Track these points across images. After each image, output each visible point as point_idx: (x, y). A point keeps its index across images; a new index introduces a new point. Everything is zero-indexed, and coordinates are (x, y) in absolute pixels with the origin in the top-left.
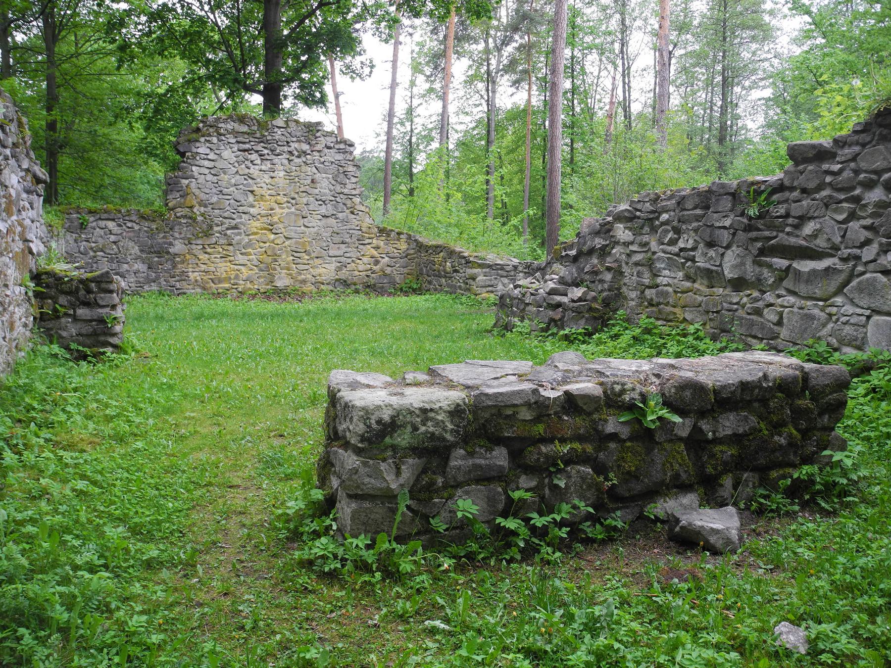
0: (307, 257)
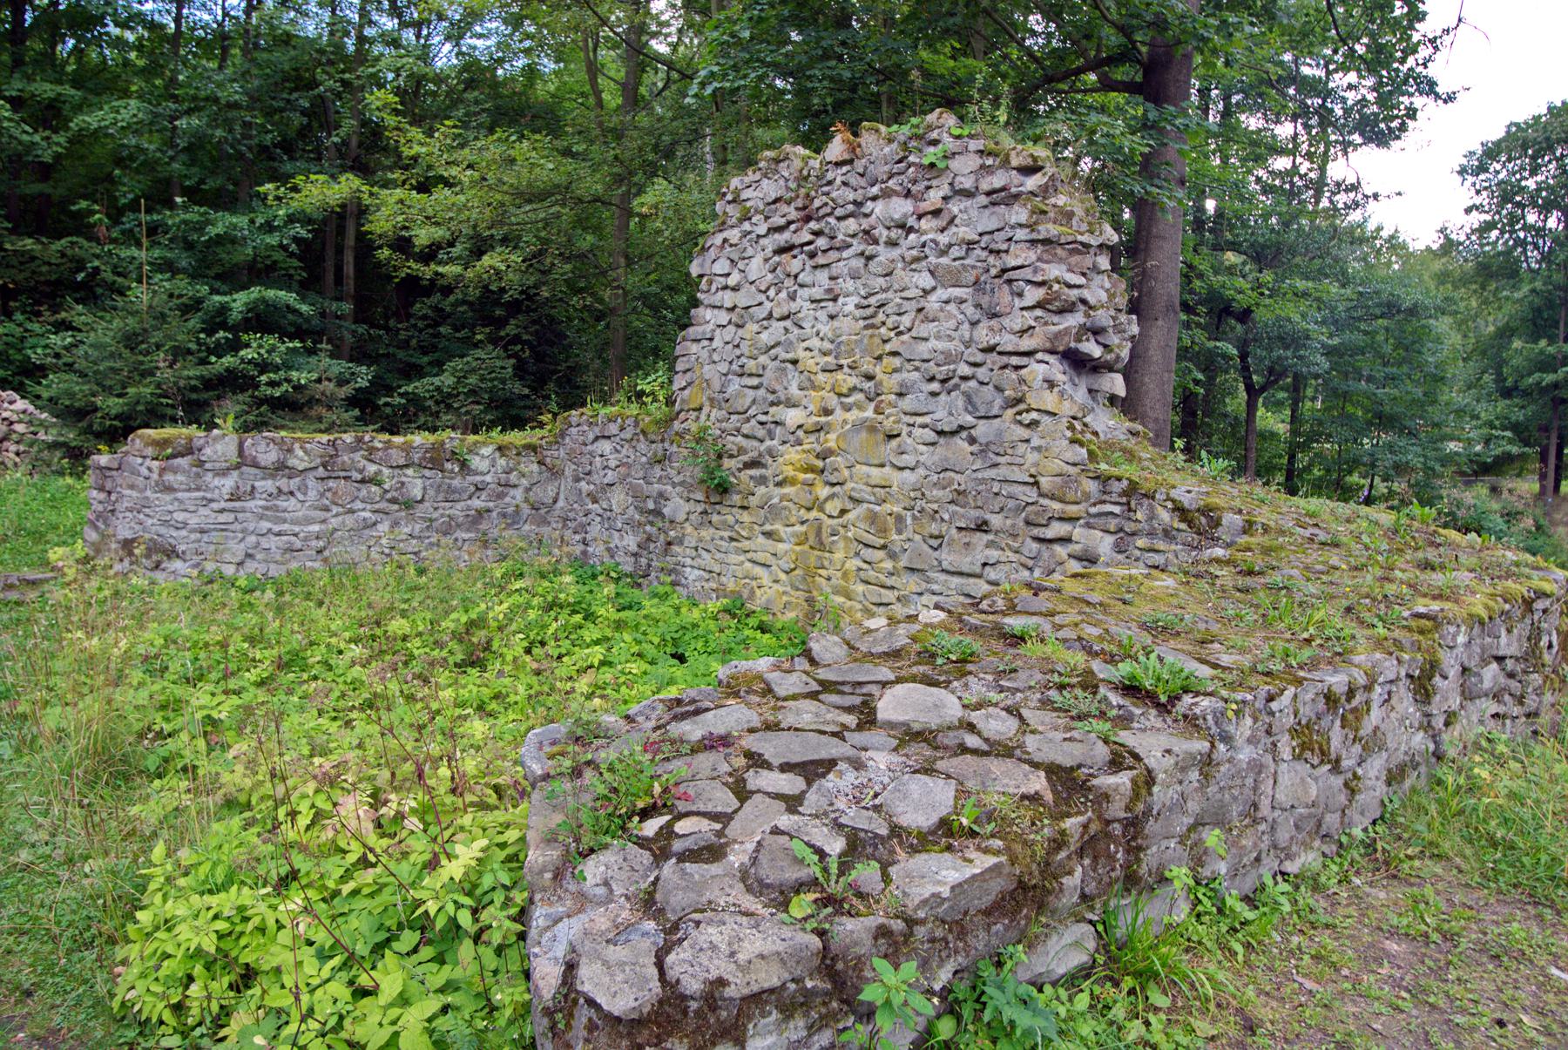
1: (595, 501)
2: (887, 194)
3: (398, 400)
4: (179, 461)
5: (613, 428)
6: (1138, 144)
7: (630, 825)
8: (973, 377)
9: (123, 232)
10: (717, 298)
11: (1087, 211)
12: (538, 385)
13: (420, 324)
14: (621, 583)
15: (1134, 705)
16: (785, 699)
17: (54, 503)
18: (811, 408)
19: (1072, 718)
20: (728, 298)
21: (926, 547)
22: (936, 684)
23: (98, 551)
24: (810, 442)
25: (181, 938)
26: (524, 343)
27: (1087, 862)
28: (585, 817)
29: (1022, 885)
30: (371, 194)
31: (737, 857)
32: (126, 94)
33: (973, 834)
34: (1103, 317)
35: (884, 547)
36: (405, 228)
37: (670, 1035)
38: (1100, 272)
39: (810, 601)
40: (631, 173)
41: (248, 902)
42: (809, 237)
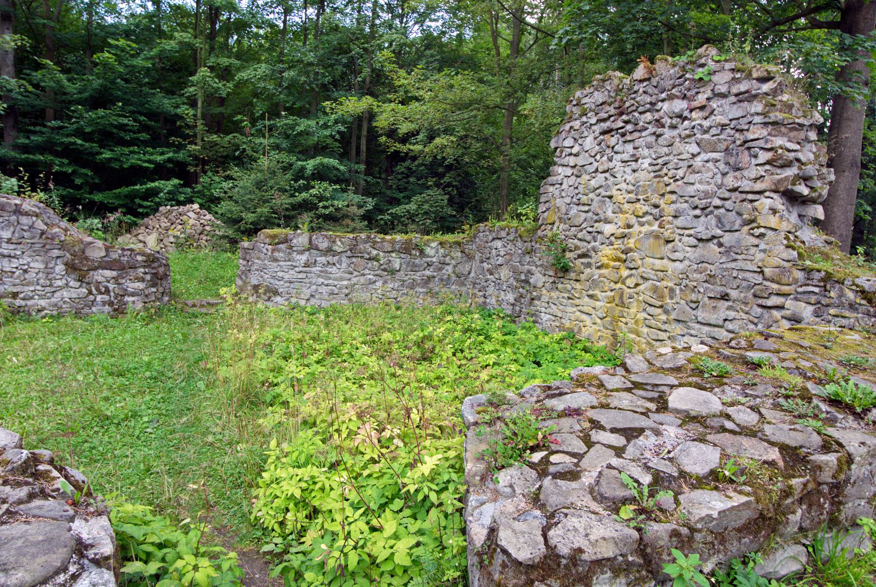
0: (664, 317)
1: (491, 274)
2: (671, 98)
3: (388, 217)
4: (281, 246)
5: (503, 234)
6: (837, 60)
7: (525, 455)
8: (722, 207)
9: (257, 130)
10: (565, 161)
11: (802, 104)
12: (461, 208)
13: (400, 177)
14: (505, 320)
15: (838, 412)
16: (612, 391)
17: (222, 266)
18: (620, 224)
19: (795, 416)
20: (572, 161)
21: (688, 308)
22: (704, 389)
23: (242, 290)
24: (618, 244)
25: (284, 488)
26: (453, 186)
27: (804, 507)
28: (500, 448)
29: (762, 516)
30: (378, 106)
31: (587, 479)
32: (259, 61)
33: (731, 481)
34: (811, 170)
35: (661, 307)
36: (393, 124)
37: (550, 576)
38: (809, 142)
39: (614, 336)
40: (516, 92)
41: (316, 474)
42: (622, 124)
